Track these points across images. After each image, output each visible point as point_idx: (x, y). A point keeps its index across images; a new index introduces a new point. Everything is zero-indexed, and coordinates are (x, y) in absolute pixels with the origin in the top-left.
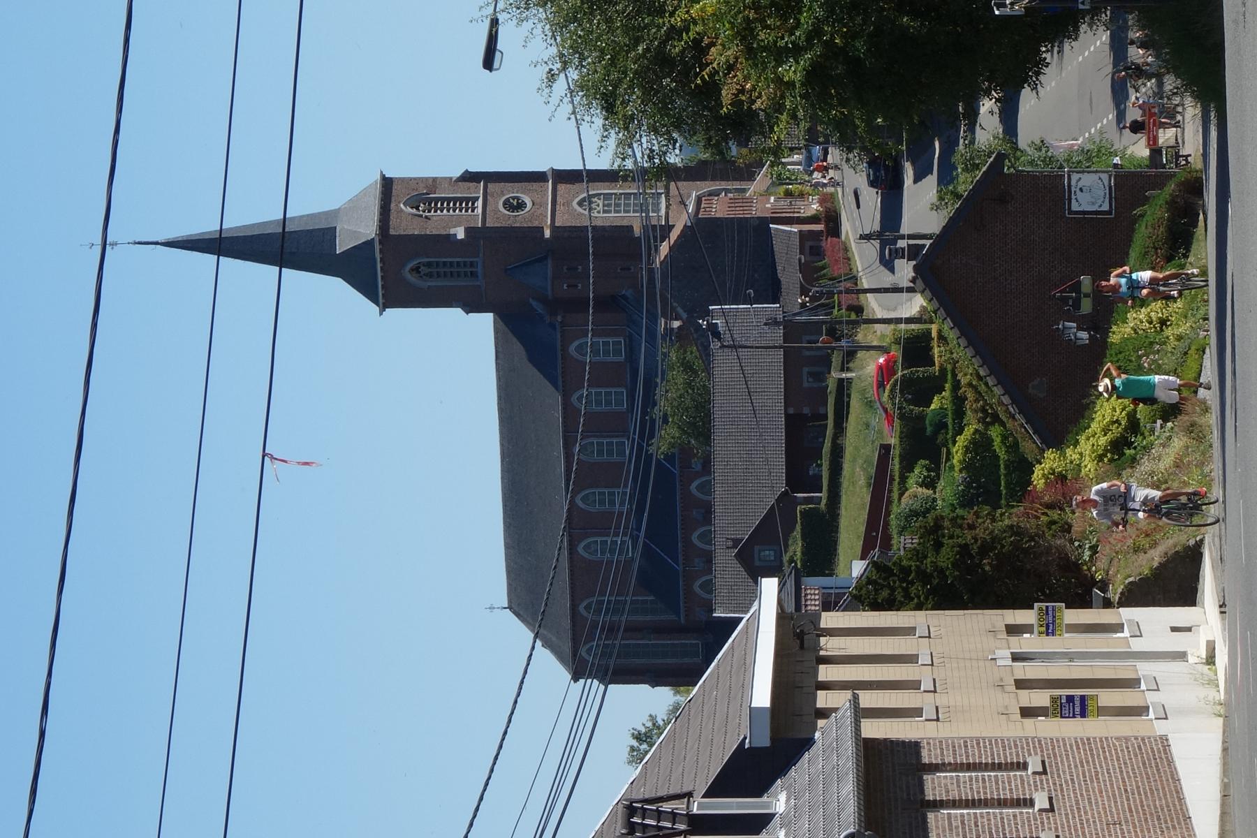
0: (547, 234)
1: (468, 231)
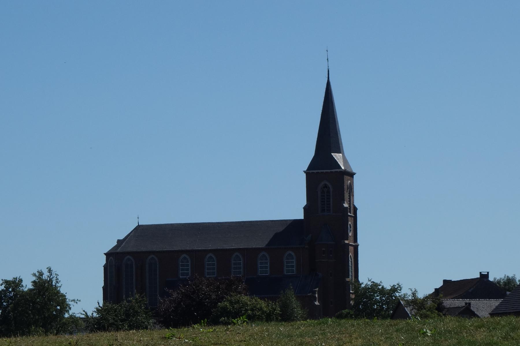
0: (346, 242)
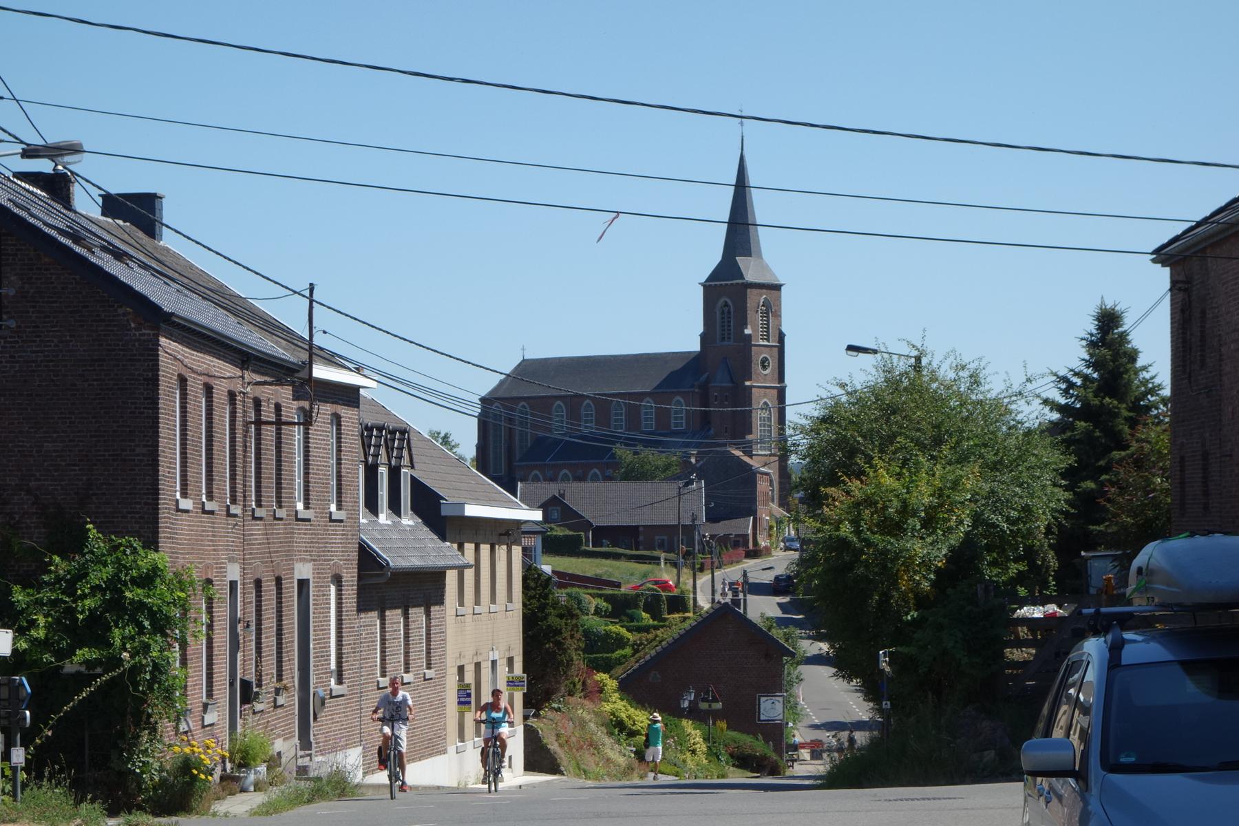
0: (748, 383)
1: (750, 336)
